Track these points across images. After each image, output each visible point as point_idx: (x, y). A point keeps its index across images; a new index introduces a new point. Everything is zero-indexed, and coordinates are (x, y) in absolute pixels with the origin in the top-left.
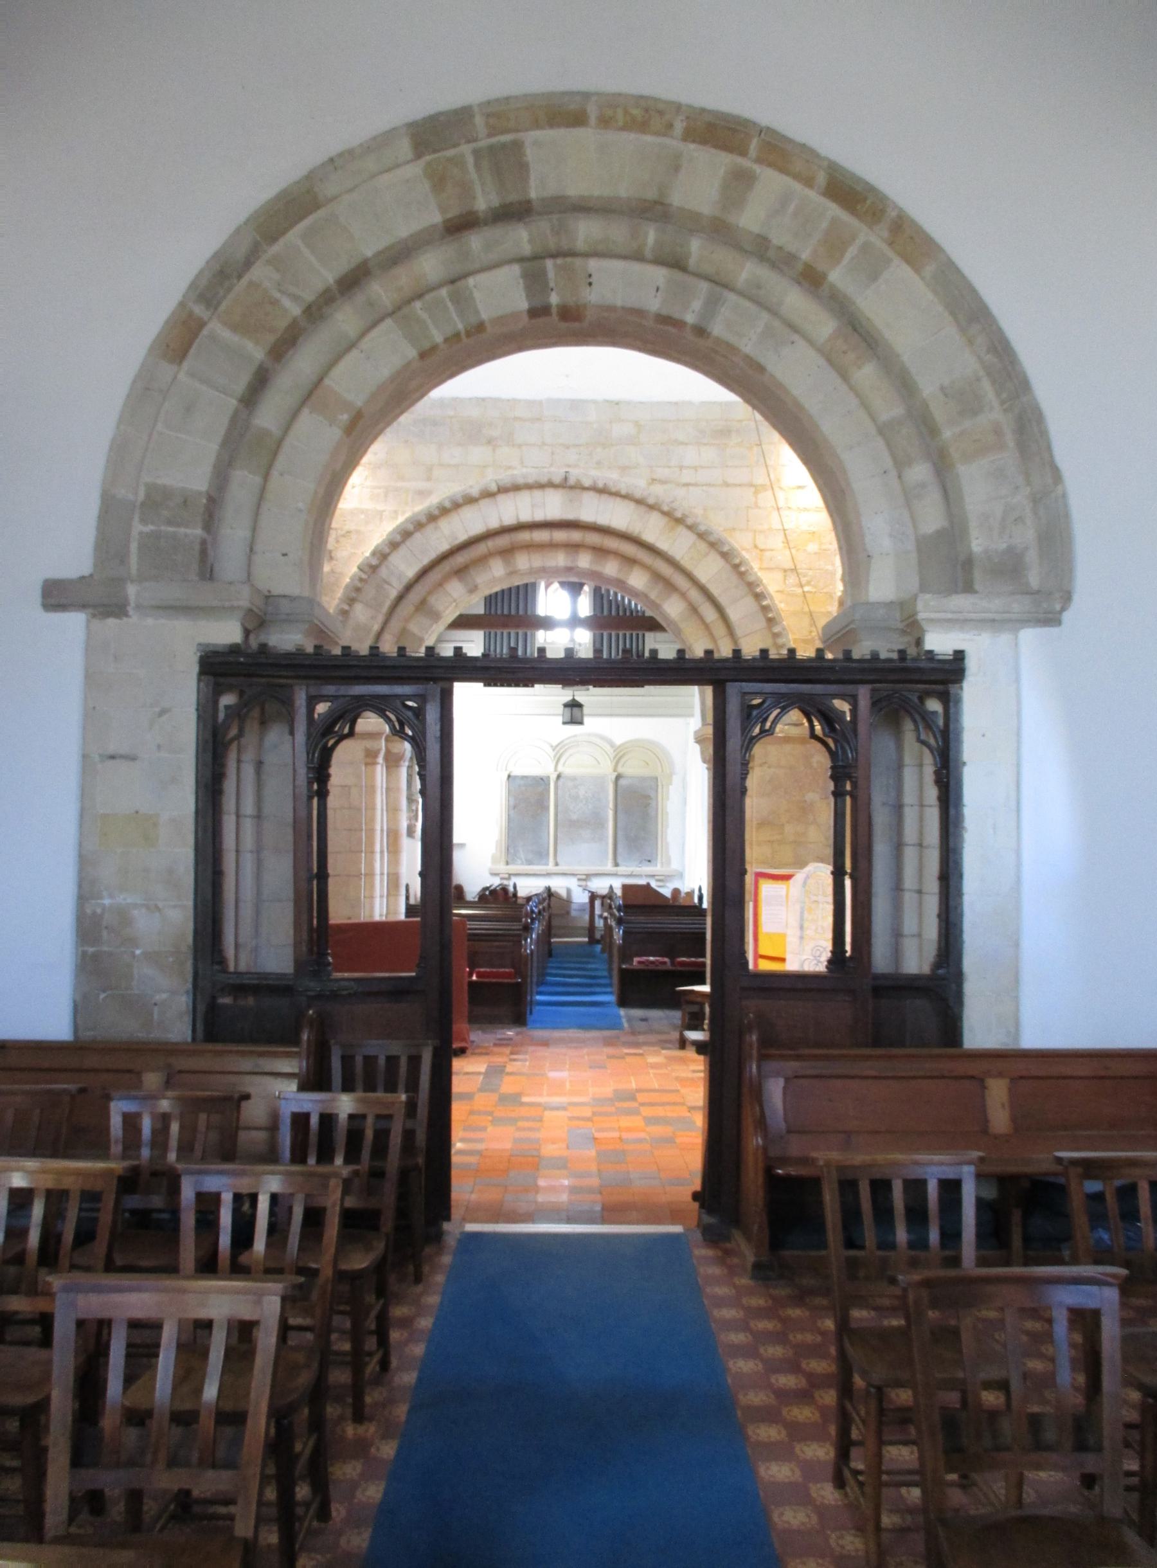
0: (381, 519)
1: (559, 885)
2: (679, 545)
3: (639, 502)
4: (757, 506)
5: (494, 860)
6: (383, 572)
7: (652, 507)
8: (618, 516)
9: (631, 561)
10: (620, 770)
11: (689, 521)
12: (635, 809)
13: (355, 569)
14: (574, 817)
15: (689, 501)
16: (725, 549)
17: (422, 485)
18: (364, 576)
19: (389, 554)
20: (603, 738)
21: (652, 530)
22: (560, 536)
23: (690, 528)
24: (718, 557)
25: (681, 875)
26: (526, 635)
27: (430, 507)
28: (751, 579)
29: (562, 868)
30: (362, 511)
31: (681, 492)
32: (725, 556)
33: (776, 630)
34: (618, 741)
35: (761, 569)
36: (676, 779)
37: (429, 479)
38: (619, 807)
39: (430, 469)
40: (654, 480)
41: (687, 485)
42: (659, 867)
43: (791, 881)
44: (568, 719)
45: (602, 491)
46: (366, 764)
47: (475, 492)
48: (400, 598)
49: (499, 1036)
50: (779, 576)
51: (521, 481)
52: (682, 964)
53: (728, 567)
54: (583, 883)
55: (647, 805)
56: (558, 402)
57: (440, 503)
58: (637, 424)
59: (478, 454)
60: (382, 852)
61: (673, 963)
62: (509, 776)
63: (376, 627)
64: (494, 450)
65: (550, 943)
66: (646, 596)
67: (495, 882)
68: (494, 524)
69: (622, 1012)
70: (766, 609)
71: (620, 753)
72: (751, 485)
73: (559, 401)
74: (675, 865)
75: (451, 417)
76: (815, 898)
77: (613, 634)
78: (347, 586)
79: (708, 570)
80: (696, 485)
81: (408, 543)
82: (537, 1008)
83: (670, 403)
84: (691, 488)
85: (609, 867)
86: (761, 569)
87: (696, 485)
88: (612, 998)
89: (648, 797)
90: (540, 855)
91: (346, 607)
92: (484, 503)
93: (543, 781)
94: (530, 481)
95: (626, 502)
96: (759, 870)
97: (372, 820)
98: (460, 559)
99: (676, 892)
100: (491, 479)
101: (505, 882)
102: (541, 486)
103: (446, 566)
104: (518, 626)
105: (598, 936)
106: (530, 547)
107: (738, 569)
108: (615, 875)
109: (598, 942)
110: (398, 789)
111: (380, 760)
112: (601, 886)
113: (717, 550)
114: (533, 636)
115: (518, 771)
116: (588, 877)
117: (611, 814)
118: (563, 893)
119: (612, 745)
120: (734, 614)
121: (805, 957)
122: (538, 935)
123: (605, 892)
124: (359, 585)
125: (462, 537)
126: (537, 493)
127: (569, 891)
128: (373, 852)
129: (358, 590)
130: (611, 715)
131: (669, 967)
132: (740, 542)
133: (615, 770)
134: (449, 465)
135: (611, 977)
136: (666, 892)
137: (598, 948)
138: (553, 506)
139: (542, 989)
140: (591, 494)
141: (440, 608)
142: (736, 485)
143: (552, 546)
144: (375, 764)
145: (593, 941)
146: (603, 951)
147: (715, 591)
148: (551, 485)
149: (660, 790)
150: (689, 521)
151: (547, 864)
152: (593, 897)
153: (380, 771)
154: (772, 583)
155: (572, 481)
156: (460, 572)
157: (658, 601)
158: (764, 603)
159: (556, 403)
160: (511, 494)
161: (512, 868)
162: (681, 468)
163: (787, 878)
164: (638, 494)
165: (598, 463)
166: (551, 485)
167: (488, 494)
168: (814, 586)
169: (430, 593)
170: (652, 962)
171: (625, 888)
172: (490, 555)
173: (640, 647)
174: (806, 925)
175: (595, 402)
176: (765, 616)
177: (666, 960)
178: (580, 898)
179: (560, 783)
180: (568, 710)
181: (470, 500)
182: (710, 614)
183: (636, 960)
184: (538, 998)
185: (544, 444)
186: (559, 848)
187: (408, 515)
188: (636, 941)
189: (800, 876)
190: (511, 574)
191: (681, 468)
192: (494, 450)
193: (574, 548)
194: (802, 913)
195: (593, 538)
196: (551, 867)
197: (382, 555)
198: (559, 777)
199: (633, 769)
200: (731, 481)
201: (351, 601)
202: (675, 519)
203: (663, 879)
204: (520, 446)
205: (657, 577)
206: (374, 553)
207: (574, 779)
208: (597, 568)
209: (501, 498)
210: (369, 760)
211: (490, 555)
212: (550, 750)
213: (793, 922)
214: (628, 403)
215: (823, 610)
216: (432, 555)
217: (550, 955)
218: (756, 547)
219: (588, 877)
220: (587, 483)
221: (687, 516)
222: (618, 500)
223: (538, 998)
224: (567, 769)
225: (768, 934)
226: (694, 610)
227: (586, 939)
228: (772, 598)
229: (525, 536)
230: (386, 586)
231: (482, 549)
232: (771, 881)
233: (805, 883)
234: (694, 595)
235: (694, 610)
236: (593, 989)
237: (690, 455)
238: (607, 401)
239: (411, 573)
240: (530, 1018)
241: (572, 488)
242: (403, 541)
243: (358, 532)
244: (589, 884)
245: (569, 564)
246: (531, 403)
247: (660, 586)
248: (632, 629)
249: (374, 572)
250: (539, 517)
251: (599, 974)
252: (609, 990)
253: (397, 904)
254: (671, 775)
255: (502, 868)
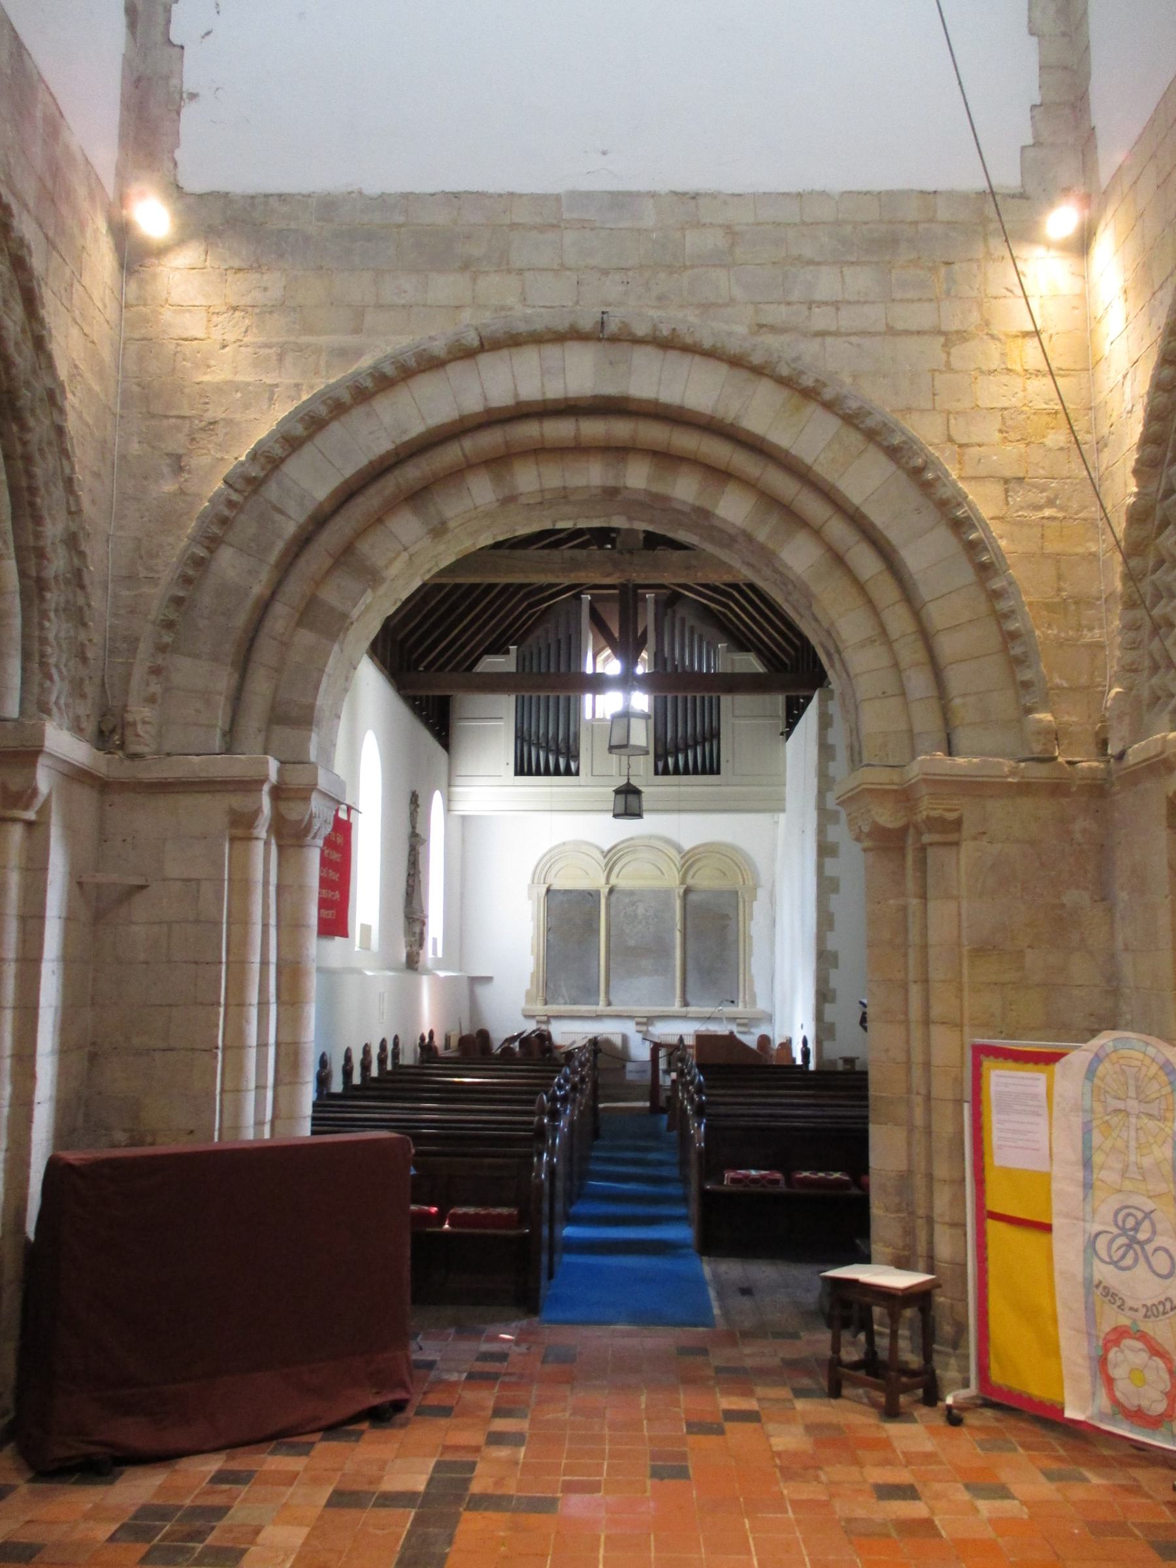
0: (271, 399)
1: (610, 1030)
2: (810, 438)
3: (736, 362)
4: (949, 367)
5: (529, 997)
6: (272, 491)
7: (758, 371)
8: (696, 388)
9: (721, 475)
10: (690, 881)
11: (828, 394)
12: (710, 929)
13: (219, 485)
14: (632, 943)
15: (831, 361)
16: (896, 440)
17: (350, 340)
18: (235, 497)
19: (283, 460)
20: (668, 842)
21: (759, 411)
22: (593, 429)
23: (828, 406)
24: (883, 459)
25: (769, 1018)
26: (568, 699)
27: (358, 374)
28: (944, 493)
29: (615, 1009)
30: (237, 387)
31: (809, 348)
32: (894, 453)
33: (997, 584)
34: (687, 845)
35: (960, 478)
36: (762, 894)
37: (357, 331)
38: (689, 931)
39: (359, 312)
40: (761, 326)
41: (822, 334)
42: (741, 1007)
43: (1058, 1067)
44: (621, 809)
45: (668, 343)
46: (233, 840)
47: (439, 347)
48: (303, 541)
49: (485, 1347)
50: (997, 490)
51: (522, 327)
52: (805, 1182)
53: (902, 476)
54: (644, 1028)
55: (725, 927)
56: (587, 197)
57: (375, 367)
58: (728, 229)
59: (446, 287)
60: (263, 1004)
61: (789, 1181)
62: (548, 890)
63: (258, 588)
64: (474, 280)
65: (595, 1109)
66: (749, 538)
67: (530, 1027)
68: (472, 404)
69: (707, 1269)
70: (973, 547)
71: (690, 860)
72: (940, 333)
73: (589, 195)
74: (762, 1005)
75: (400, 226)
76: (1120, 1105)
77: (680, 696)
78: (204, 515)
79: (865, 481)
80: (836, 334)
81: (320, 440)
82: (568, 1258)
83: (786, 195)
84: (829, 340)
85: (677, 1007)
86: (960, 478)
87: (836, 334)
88: (683, 1233)
89: (725, 917)
90: (588, 993)
91: (202, 553)
92: (454, 369)
93: (591, 896)
94: (538, 326)
95: (713, 364)
96: (980, 1041)
97: (239, 945)
98: (412, 474)
99: (764, 1040)
100: (470, 323)
101: (544, 1027)
102: (560, 337)
103: (389, 485)
104: (553, 688)
105: (662, 1101)
106: (541, 451)
107: (919, 475)
108: (684, 1017)
109: (663, 1111)
110: (302, 888)
111: (262, 831)
112: (669, 1031)
113: (879, 445)
114: (579, 703)
115: (558, 885)
116: (650, 1020)
117: (678, 936)
118: (618, 1041)
119: (679, 849)
120: (914, 559)
121: (1096, 1228)
122: (571, 1124)
123: (674, 1040)
124: (226, 512)
125: (416, 429)
126: (552, 351)
127: (625, 1038)
128: (242, 1004)
129: (224, 522)
130: (679, 811)
131: (782, 1188)
132: (925, 431)
133: (683, 882)
134: (391, 307)
135: (684, 1180)
136: (750, 1040)
137: (664, 1120)
138: (578, 373)
139: (579, 1209)
140: (650, 350)
141: (381, 563)
142: (907, 333)
143: (579, 449)
144: (250, 838)
145: (655, 1109)
146: (670, 1128)
147: (877, 516)
148: (574, 335)
149: (741, 906)
150: (828, 394)
151: (598, 1004)
152: (656, 1048)
153: (262, 857)
154: (984, 502)
155: (613, 327)
156: (416, 497)
157: (771, 545)
158: (973, 536)
159: (583, 198)
160: (505, 352)
161: (553, 1009)
162: (810, 304)
163: (1049, 1059)
164: (733, 347)
165: (660, 298)
166: (574, 335)
167: (465, 353)
168: (1061, 508)
169: (360, 534)
170: (755, 1181)
171: (701, 1039)
172: (469, 466)
173: (715, 724)
174: (1098, 1158)
175: (653, 195)
176: (971, 560)
177: (778, 1176)
178: (641, 1052)
179: (613, 898)
180: (621, 797)
181: (430, 363)
182: (867, 563)
183: (729, 1175)
184: (569, 1231)
185: (564, 267)
186: (611, 984)
187: (320, 385)
188: (729, 1144)
189: (1079, 1057)
190: (509, 500)
191: (810, 304)
192: (474, 280)
193: (618, 452)
194: (1087, 1130)
195: (654, 433)
196: (601, 1007)
197: (271, 460)
198: (611, 891)
199: (704, 880)
200: (900, 326)
201: (213, 543)
202: (805, 392)
203: (748, 1023)
204: (520, 272)
205: (770, 501)
206: (254, 456)
207: (631, 893)
208: (658, 488)
209: (484, 359)
210: (239, 832)
211: (469, 466)
212: (599, 856)
213: (1068, 1151)
214: (714, 196)
215: (1080, 550)
216: (361, 461)
217: (596, 1134)
218: (950, 439)
219: (650, 1020)
220: (641, 330)
221: (825, 385)
222: (697, 358)
223: (569, 1231)
224: (622, 881)
225: (1007, 1171)
226: (838, 559)
227: (648, 1104)
228: (986, 528)
229: (530, 430)
230: (277, 517)
231: (451, 454)
232: (1010, 1064)
233: (1091, 1073)
234: (837, 529)
235: (838, 559)
236: (653, 1210)
237: (827, 283)
238: (675, 193)
239: (322, 491)
240: (547, 1289)
241: (614, 339)
242: (310, 437)
243: (229, 422)
244: (650, 1029)
245: (611, 482)
246: (539, 200)
247: (774, 520)
248: (709, 691)
249: (255, 491)
250: (555, 390)
251: (665, 1172)
252: (680, 1211)
253: (294, 1100)
254: (755, 888)
255: (539, 1008)
